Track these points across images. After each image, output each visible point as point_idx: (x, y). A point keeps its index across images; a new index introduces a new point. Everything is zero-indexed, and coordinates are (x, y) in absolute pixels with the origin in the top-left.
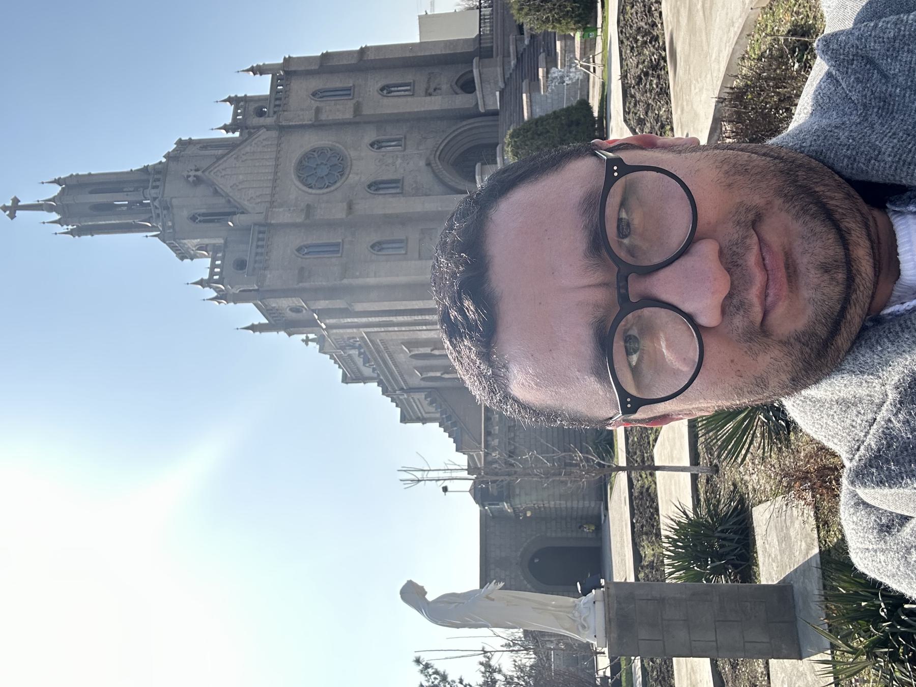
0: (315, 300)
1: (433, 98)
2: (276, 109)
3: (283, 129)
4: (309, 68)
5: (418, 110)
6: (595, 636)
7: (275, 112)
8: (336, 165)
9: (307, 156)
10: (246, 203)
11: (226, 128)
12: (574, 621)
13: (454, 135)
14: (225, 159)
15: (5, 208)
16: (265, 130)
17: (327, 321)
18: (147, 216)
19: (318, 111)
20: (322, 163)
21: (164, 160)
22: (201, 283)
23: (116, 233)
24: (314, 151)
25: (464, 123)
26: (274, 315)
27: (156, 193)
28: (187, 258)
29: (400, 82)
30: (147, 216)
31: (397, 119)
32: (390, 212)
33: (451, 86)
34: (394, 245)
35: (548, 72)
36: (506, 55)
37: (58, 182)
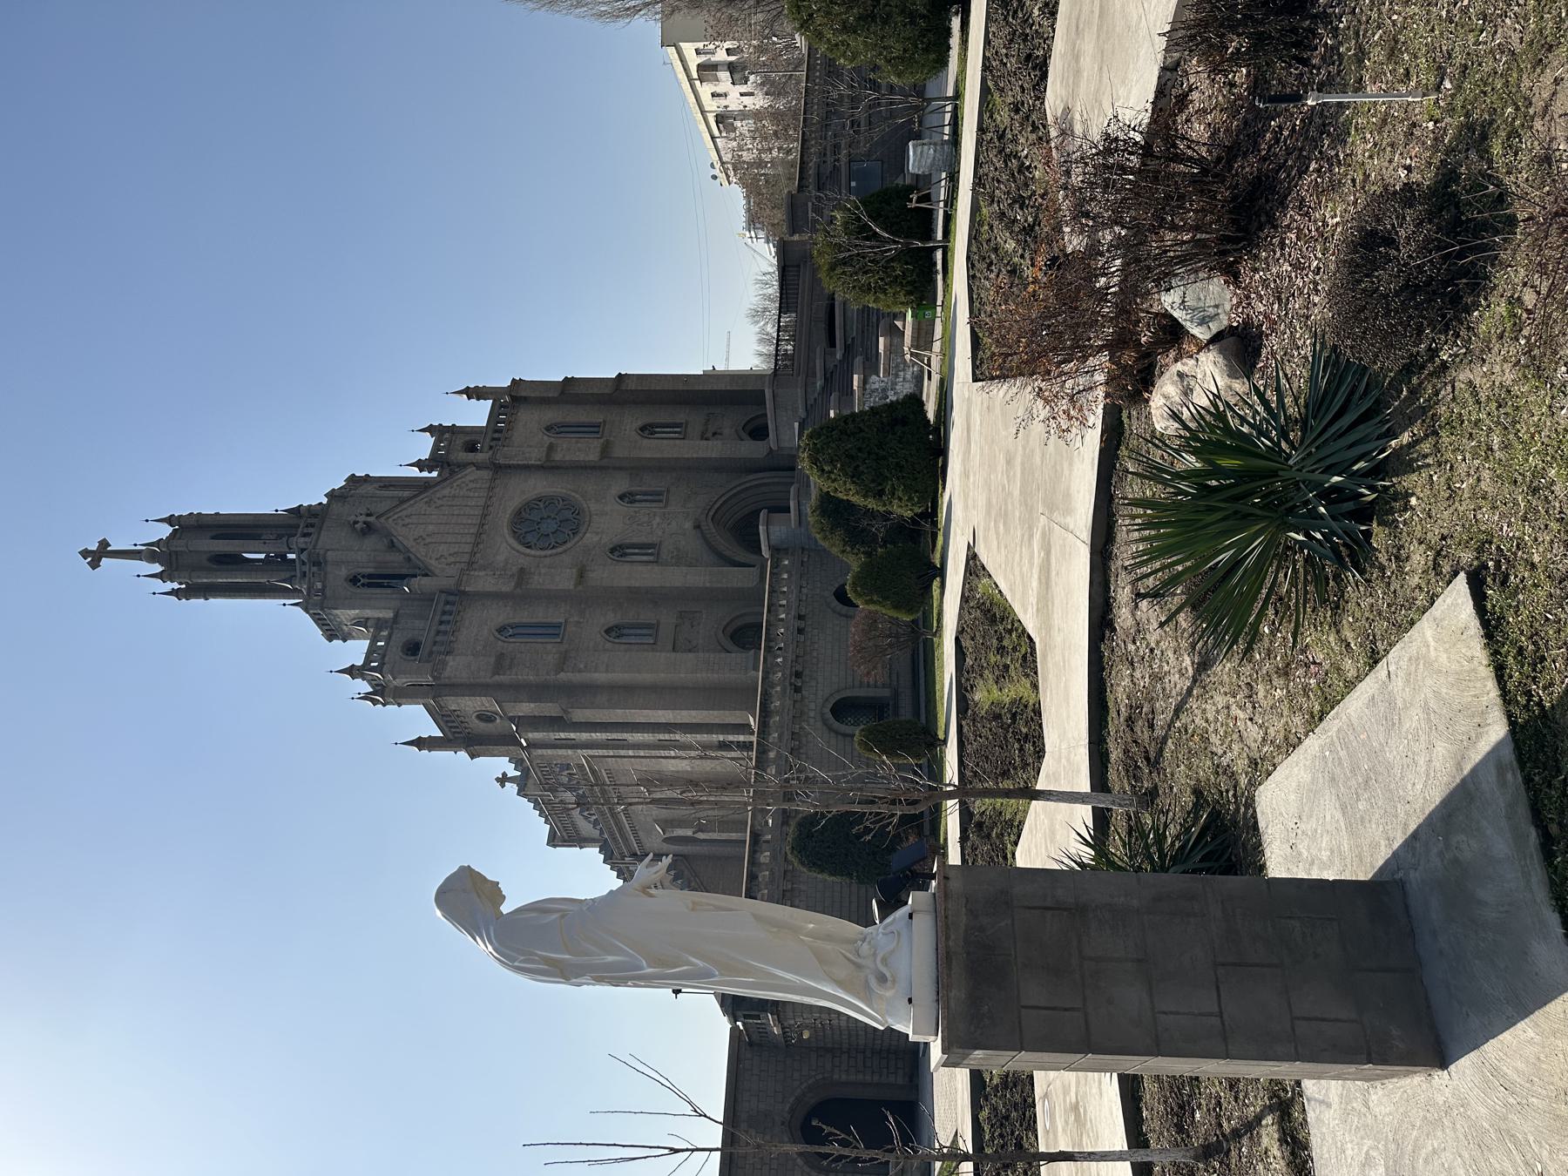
0: (515, 702)
1: (710, 443)
2: (493, 444)
3: (498, 469)
4: (545, 395)
5: (690, 456)
6: (910, 1001)
7: (491, 447)
8: (567, 520)
9: (529, 506)
10: (433, 562)
12: (859, 966)
13: (735, 491)
14: (412, 502)
17: (531, 735)
18: (288, 575)
19: (551, 448)
20: (549, 517)
21: (325, 501)
22: (352, 671)
23: (240, 597)
25: (751, 477)
26: (448, 719)
27: (306, 543)
28: (338, 638)
29: (669, 420)
30: (288, 575)
31: (660, 467)
32: (637, 585)
33: (736, 431)
34: (639, 631)
35: (865, 382)
36: (810, 373)
37: (170, 520)
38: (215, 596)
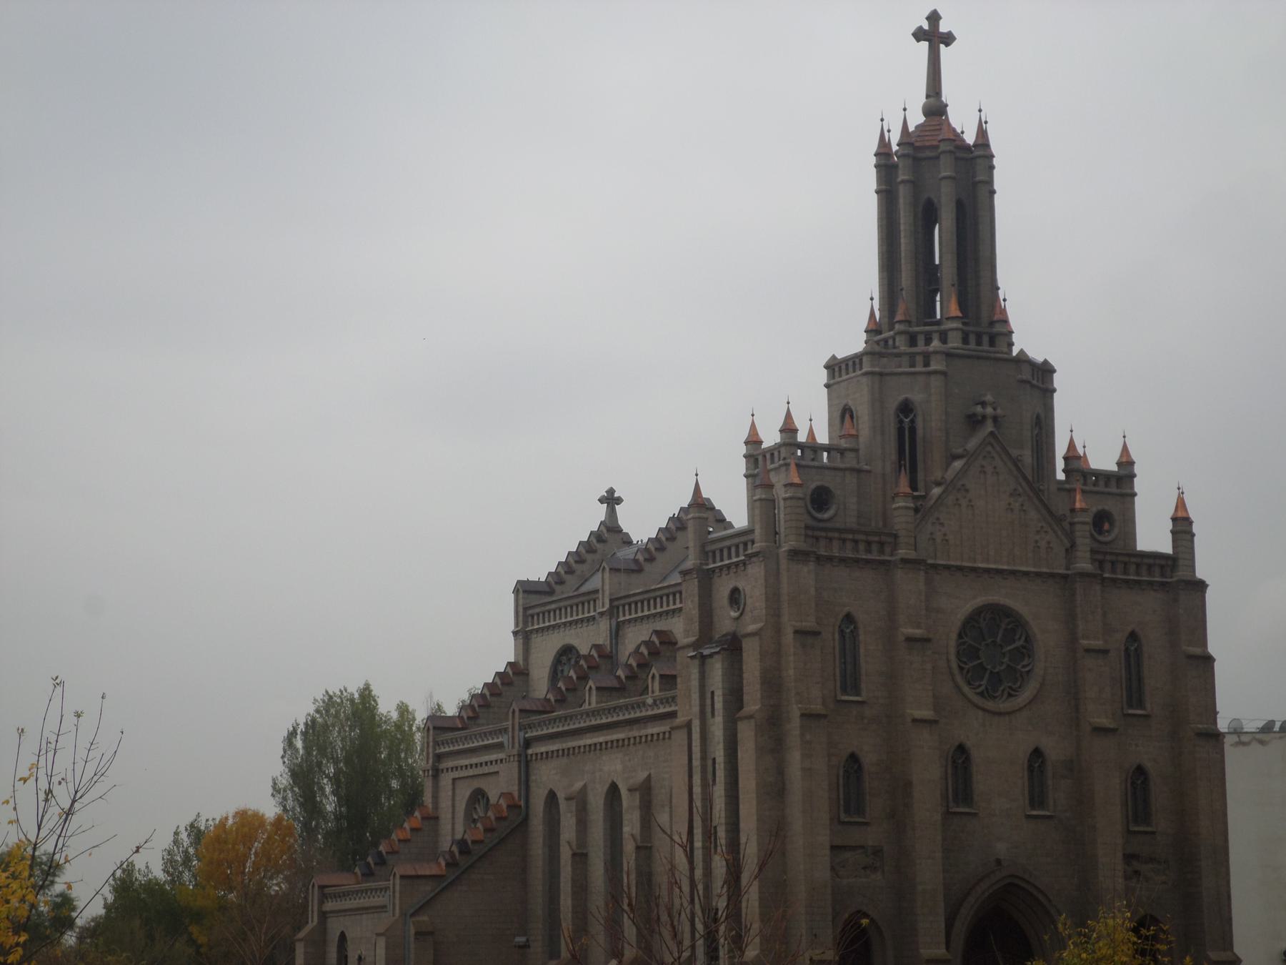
11: (1072, 445)
15: (934, 18)
21: (1015, 352)
24: (1026, 641)
37: (982, 133)
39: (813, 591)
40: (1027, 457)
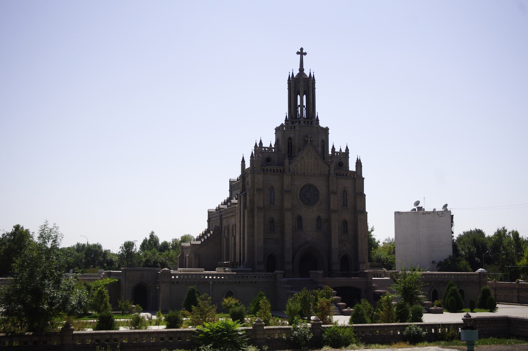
11: (333, 148)
16: (328, 170)
19: (336, 193)
38: (288, 90)
39: (262, 181)
40: (320, 149)
